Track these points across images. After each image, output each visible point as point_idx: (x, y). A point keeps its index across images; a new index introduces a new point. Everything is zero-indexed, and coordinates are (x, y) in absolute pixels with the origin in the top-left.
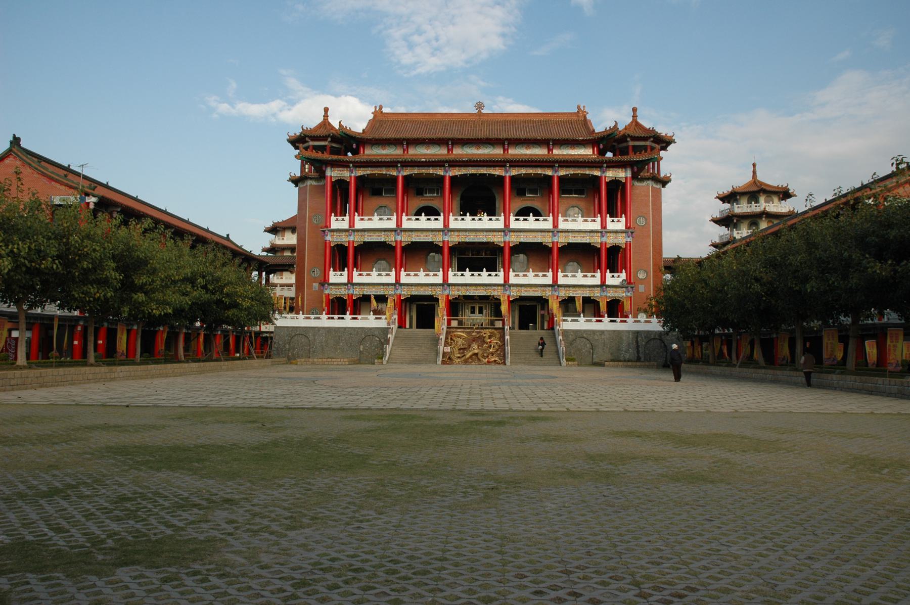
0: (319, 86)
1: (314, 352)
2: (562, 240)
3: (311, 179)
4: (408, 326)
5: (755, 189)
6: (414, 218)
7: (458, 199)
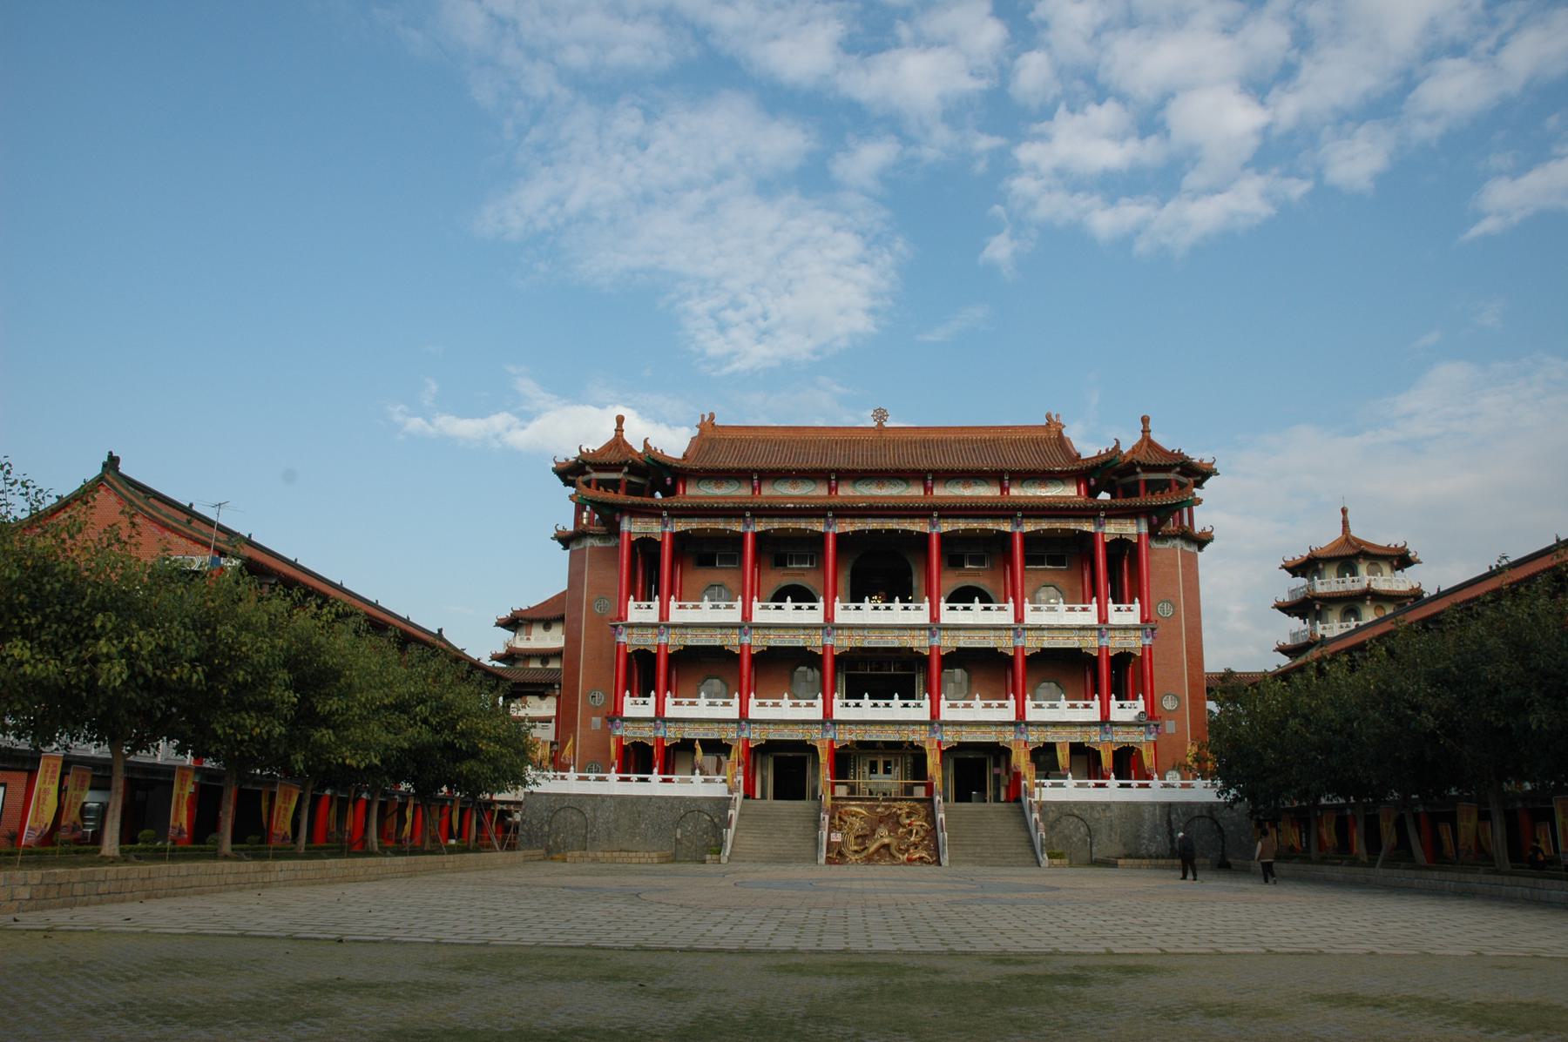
0: (572, 391)
1: (594, 839)
2: (1032, 643)
3: (592, 536)
4: (758, 795)
5: (1350, 552)
6: (773, 605)
7: (847, 573)
